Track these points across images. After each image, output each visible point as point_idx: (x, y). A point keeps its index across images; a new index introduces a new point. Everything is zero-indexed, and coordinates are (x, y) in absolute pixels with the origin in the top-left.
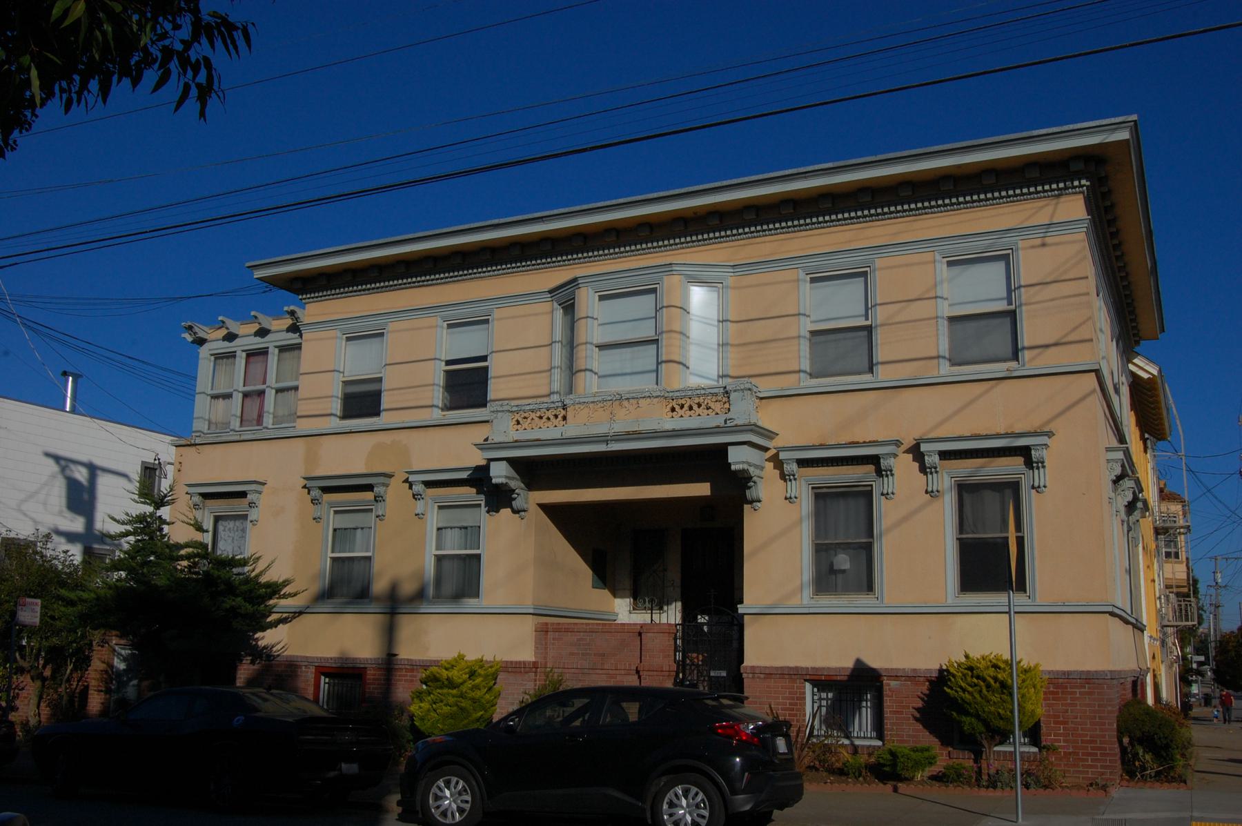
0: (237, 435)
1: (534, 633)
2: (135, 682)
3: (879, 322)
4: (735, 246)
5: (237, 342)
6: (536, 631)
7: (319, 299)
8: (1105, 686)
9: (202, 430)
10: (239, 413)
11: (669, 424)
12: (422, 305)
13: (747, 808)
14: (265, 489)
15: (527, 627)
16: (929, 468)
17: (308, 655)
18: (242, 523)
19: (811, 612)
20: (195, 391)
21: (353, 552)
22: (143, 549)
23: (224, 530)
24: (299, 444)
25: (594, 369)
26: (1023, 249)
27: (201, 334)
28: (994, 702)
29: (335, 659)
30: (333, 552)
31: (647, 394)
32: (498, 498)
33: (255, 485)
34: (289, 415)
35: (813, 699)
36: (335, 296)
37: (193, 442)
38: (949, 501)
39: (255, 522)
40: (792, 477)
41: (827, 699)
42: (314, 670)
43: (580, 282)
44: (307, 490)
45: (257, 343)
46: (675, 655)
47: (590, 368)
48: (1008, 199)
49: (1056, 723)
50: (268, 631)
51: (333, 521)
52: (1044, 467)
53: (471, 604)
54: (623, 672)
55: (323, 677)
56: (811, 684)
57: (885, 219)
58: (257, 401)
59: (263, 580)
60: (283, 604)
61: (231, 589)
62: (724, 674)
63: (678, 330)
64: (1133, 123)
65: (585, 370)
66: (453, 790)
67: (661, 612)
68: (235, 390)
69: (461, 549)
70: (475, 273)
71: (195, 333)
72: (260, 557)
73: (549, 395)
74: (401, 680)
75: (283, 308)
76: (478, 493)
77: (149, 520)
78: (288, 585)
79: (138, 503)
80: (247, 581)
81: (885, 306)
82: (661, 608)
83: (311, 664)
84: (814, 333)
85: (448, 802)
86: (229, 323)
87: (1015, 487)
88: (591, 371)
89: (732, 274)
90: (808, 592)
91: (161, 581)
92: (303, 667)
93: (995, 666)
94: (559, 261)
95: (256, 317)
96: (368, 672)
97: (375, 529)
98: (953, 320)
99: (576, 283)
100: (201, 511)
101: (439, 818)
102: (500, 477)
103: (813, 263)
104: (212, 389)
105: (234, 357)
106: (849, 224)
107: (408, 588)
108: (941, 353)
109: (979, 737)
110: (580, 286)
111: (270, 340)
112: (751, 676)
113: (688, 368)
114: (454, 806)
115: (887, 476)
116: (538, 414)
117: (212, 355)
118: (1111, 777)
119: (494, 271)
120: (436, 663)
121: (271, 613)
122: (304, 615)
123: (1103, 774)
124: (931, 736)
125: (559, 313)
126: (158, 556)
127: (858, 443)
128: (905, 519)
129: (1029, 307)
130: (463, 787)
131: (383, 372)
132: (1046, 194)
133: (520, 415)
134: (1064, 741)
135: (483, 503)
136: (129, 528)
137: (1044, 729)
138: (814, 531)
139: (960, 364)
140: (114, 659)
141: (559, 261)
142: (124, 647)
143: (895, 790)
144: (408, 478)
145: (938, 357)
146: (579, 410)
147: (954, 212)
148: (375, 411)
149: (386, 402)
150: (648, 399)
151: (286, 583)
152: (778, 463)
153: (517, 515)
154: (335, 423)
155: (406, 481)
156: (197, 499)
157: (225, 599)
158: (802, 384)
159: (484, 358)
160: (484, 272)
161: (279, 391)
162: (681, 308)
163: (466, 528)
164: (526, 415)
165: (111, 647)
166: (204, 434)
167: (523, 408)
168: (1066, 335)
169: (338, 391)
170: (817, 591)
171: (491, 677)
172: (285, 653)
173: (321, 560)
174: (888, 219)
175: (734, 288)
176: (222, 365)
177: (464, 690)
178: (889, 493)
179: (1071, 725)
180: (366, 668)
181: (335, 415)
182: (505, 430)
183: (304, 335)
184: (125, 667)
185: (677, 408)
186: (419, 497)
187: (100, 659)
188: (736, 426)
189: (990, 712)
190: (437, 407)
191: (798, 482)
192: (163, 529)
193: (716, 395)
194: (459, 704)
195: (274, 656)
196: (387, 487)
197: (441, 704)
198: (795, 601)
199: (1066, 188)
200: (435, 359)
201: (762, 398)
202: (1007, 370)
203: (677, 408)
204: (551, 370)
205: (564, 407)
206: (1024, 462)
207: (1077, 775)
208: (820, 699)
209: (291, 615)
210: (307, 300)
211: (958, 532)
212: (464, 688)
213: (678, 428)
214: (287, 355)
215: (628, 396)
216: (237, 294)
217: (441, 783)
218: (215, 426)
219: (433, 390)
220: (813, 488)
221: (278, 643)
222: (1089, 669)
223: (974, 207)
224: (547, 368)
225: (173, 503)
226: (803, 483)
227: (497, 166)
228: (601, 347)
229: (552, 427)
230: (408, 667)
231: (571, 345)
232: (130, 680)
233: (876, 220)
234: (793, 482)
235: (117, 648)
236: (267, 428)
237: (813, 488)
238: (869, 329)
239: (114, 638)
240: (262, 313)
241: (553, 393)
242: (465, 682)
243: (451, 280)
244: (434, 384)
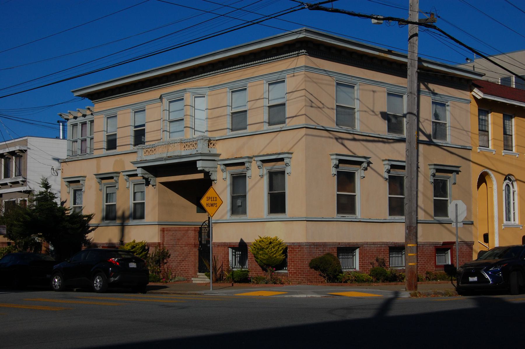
5: (78, 119)
9: (70, 155)
10: (80, 148)
12: (144, 100)
14: (86, 179)
21: (113, 202)
25: (168, 130)
30: (107, 202)
33: (81, 178)
38: (266, 180)
39: (250, 177)
41: (239, 254)
47: (166, 130)
50: (89, 233)
54: (171, 245)
60: (93, 222)
64: (305, 30)
68: (87, 137)
75: (85, 107)
78: (94, 215)
81: (251, 102)
89: (209, 91)
90: (229, 213)
95: (79, 111)
98: (270, 107)
100: (225, 173)
102: (140, 174)
111: (87, 118)
122: (99, 227)
127: (237, 158)
134: (294, 268)
140: (49, 246)
159: (144, 125)
162: (190, 106)
166: (71, 156)
169: (105, 139)
172: (93, 242)
187: (44, 246)
202: (281, 128)
211: (268, 191)
216: (72, 101)
220: (231, 174)
236: (88, 154)
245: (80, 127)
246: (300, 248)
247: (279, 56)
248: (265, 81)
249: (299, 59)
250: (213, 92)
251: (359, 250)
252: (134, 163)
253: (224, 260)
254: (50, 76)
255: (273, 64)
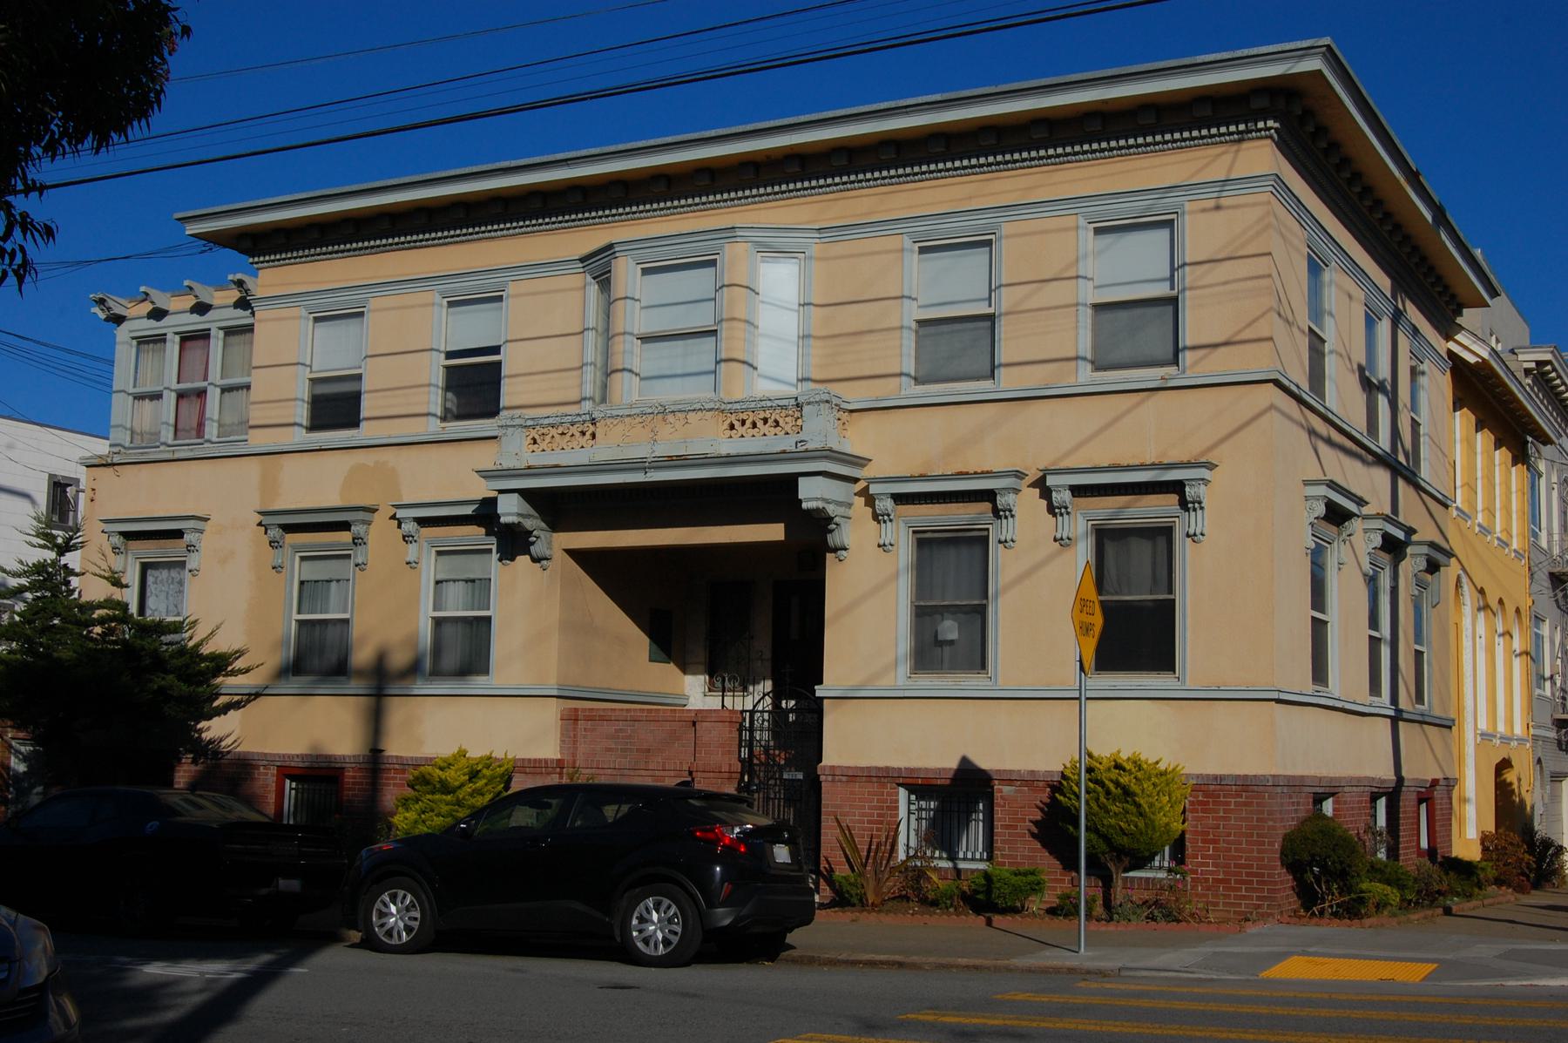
0: (169, 451)
1: (560, 721)
2: (39, 789)
3: (1003, 310)
4: (824, 201)
5: (167, 321)
6: (561, 719)
7: (276, 263)
8: (1267, 794)
9: (123, 443)
10: (172, 421)
11: (727, 446)
13: (727, 922)
14: (207, 526)
15: (550, 713)
16: (1058, 508)
17: (267, 751)
18: (179, 573)
19: (906, 695)
20: (111, 387)
21: (326, 612)
22: (44, 609)
23: (155, 583)
24: (253, 467)
25: (634, 370)
26: (1191, 212)
27: (118, 310)
28: (1115, 813)
29: (303, 757)
30: (299, 612)
31: (698, 406)
32: (513, 542)
33: (192, 522)
34: (241, 423)
35: (909, 810)
36: (303, 259)
37: (109, 461)
38: (1083, 552)
40: (1063, 510)
42: (275, 772)
43: (617, 249)
44: (263, 528)
45: (194, 322)
46: (740, 752)
47: (629, 367)
48: (1174, 145)
49: (1204, 841)
50: (216, 719)
51: (298, 571)
52: (1202, 508)
53: (478, 683)
54: (672, 773)
55: (288, 782)
56: (906, 789)
57: (1017, 169)
58: (196, 404)
59: (206, 650)
60: (230, 684)
61: (159, 663)
62: (800, 776)
63: (742, 317)
64: (1325, 48)
65: (624, 370)
66: (400, 905)
67: (745, 694)
68: (165, 388)
69: (467, 610)
70: (502, 230)
71: (109, 309)
72: (196, 621)
73: (579, 402)
74: (388, 785)
76: (487, 534)
77: (51, 570)
78: (239, 657)
79: (35, 547)
80: (183, 651)
82: (745, 689)
83: (272, 763)
84: (922, 323)
85: (394, 919)
86: (153, 293)
87: (1166, 532)
88: (630, 371)
89: (818, 240)
90: (904, 668)
91: (65, 653)
92: (262, 768)
93: (1118, 766)
94: (594, 218)
95: (191, 288)
96: (346, 774)
97: (354, 584)
98: (1099, 308)
99: (612, 251)
100: (123, 556)
101: (383, 938)
103: (921, 228)
104: (135, 386)
105: (164, 341)
106: (969, 175)
107: (399, 659)
108: (1081, 353)
109: (1103, 858)
110: (617, 255)
111: (210, 319)
112: (830, 778)
113: (756, 368)
114: (401, 925)
115: (1195, 510)
116: (560, 431)
117: (133, 338)
118: (1269, 911)
119: (508, 229)
120: (429, 761)
121: (218, 695)
123: (1259, 906)
124: (1051, 857)
125: (593, 289)
126: (64, 619)
127: (967, 473)
128: (1028, 574)
129: (1194, 292)
130: (412, 901)
131: (363, 367)
132: (1222, 139)
133: (537, 432)
134: (1215, 865)
135: (494, 548)
136: (24, 581)
137: (1190, 850)
138: (914, 588)
139: (1105, 369)
141: (594, 218)
142: (23, 742)
143: (989, 923)
144: (395, 514)
145: (1077, 358)
146: (611, 426)
147: (1106, 160)
148: (353, 421)
149: (367, 407)
150: (700, 413)
151: (239, 653)
152: (870, 501)
153: (538, 564)
154: (300, 437)
155: (393, 517)
156: (117, 540)
157: (152, 677)
158: (903, 392)
159: (495, 350)
160: (496, 231)
161: (226, 390)
162: (747, 287)
163: (473, 581)
164: (545, 431)
165: (6, 741)
166: (125, 448)
167: (541, 422)
168: (1240, 332)
170: (916, 669)
171: (498, 779)
172: (238, 749)
173: (286, 621)
174: (1021, 168)
175: (819, 259)
176: (148, 352)
177: (461, 796)
178: (1197, 533)
179: (1222, 845)
180: (344, 768)
181: (300, 425)
182: (516, 451)
183: (256, 313)
184: (26, 769)
185: (737, 424)
186: (411, 539)
188: (806, 451)
189: (1110, 826)
190: (435, 415)
191: (1071, 516)
192: (69, 582)
193: (783, 407)
194: (454, 813)
195: (222, 753)
196: (369, 525)
197: (431, 814)
198: (886, 681)
199: (1249, 131)
200: (432, 350)
201: (852, 411)
203: (737, 424)
204: (581, 367)
205: (593, 422)
206: (1179, 500)
207: (1228, 909)
208: (920, 809)
209: (245, 698)
210: (260, 265)
212: (461, 794)
213: (733, 452)
214: (234, 339)
215: (673, 408)
217: (386, 897)
218: (139, 437)
219: (429, 393)
220: (914, 532)
221: (228, 736)
222: (1247, 773)
223: (1130, 155)
224: (578, 364)
225: (82, 547)
226: (902, 525)
227: (393, 132)
228: (646, 339)
229: (577, 448)
230: (397, 766)
231: (608, 335)
232: (33, 786)
233: (1005, 170)
234: (889, 523)
235: (14, 743)
237: (914, 532)
238: (991, 318)
239: (9, 729)
240: (198, 282)
241: (585, 399)
242: (462, 785)
243: (452, 240)
244: (429, 385)
245: (177, 348)
246: (1244, 794)
247: (348, 246)
248: (437, 295)
249: (1241, 153)
250: (839, 249)
251: (1334, 803)
252: (486, 475)
253: (878, 830)
254: (431, 89)
255: (1177, 155)
